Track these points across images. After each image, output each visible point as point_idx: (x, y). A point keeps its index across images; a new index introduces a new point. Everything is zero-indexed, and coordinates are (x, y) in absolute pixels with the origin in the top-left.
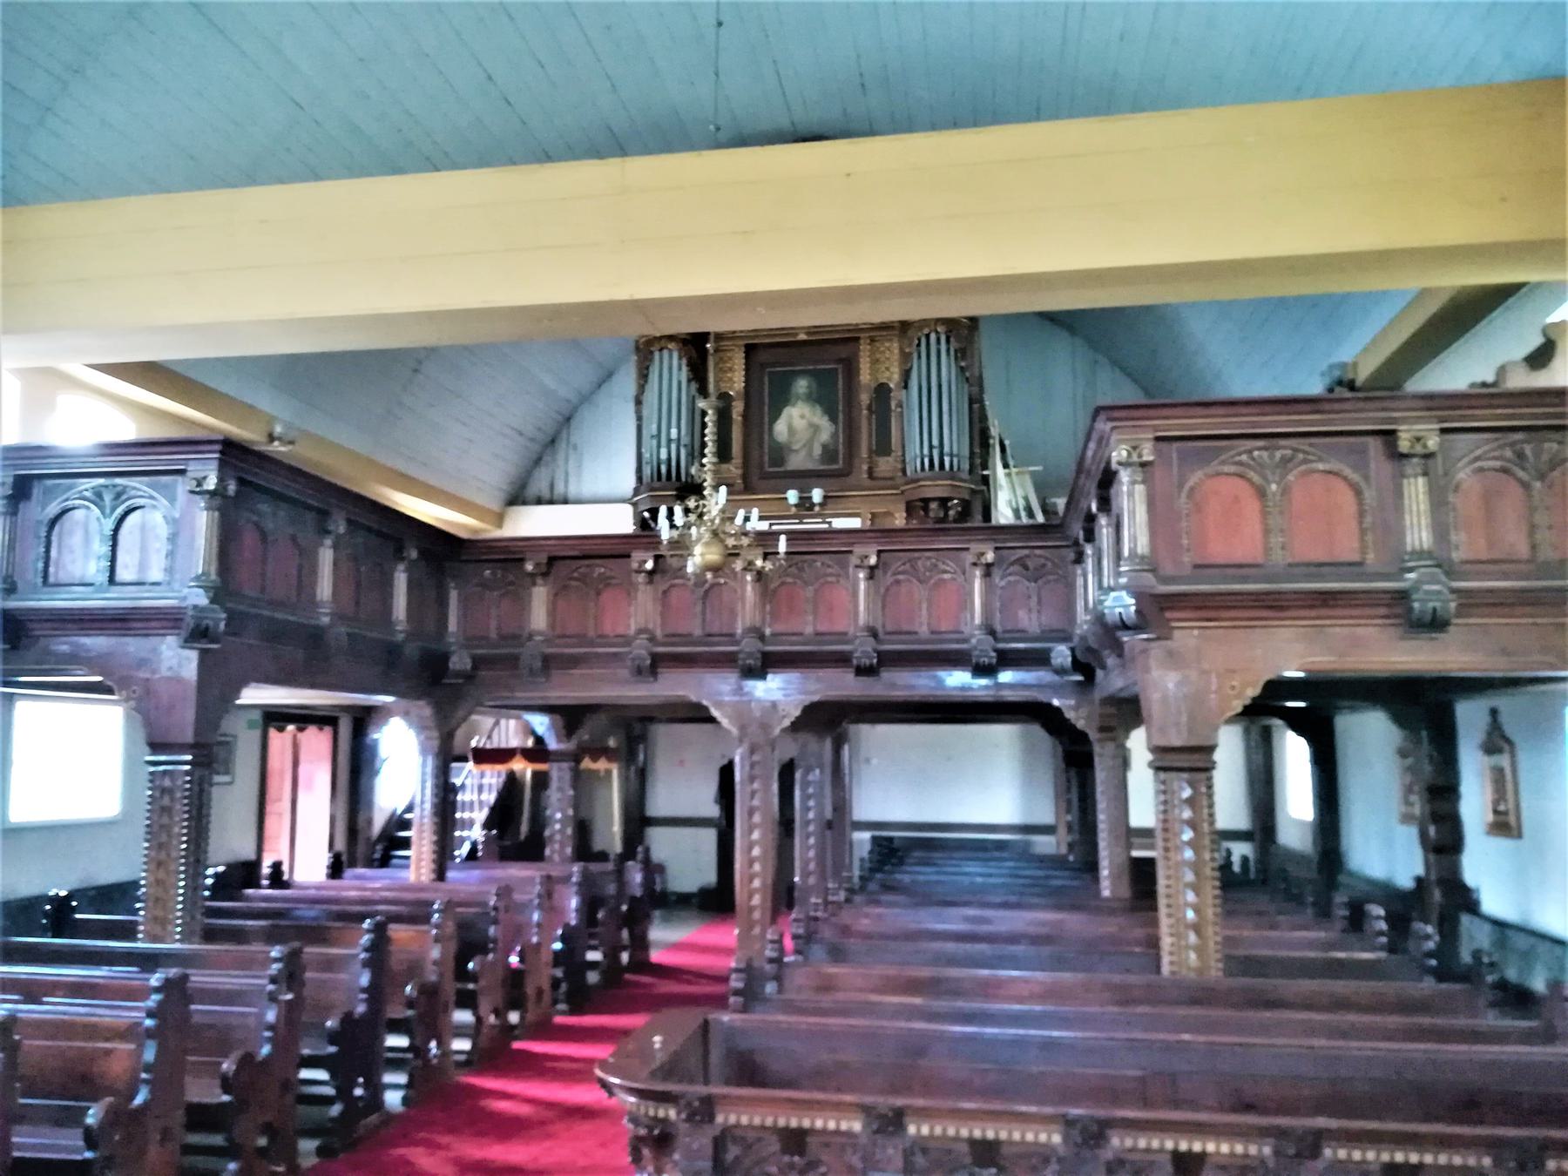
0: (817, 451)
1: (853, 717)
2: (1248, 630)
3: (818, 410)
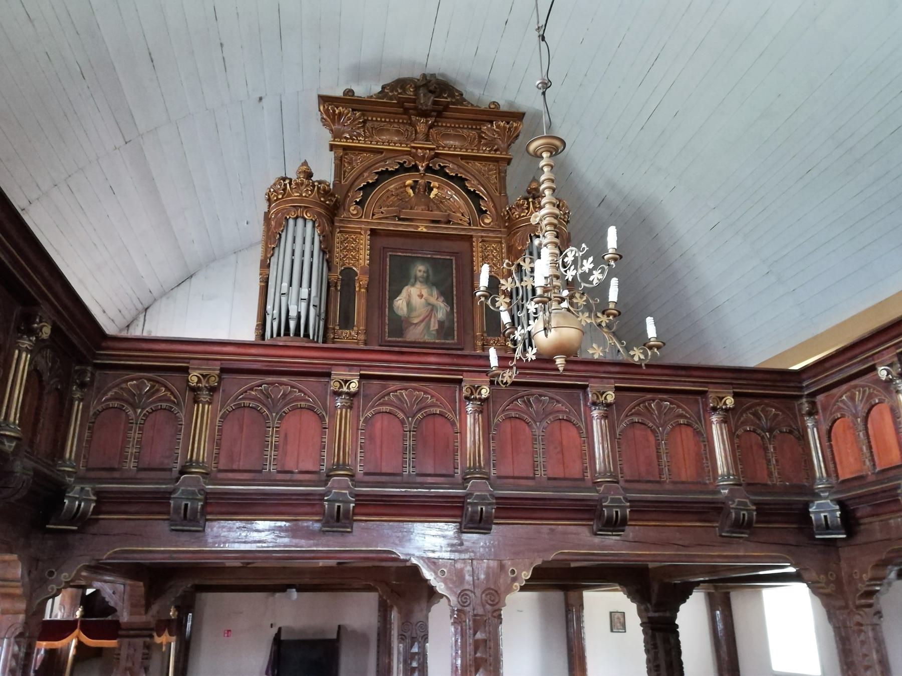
0: (434, 326)
2: (663, 527)
3: (435, 292)
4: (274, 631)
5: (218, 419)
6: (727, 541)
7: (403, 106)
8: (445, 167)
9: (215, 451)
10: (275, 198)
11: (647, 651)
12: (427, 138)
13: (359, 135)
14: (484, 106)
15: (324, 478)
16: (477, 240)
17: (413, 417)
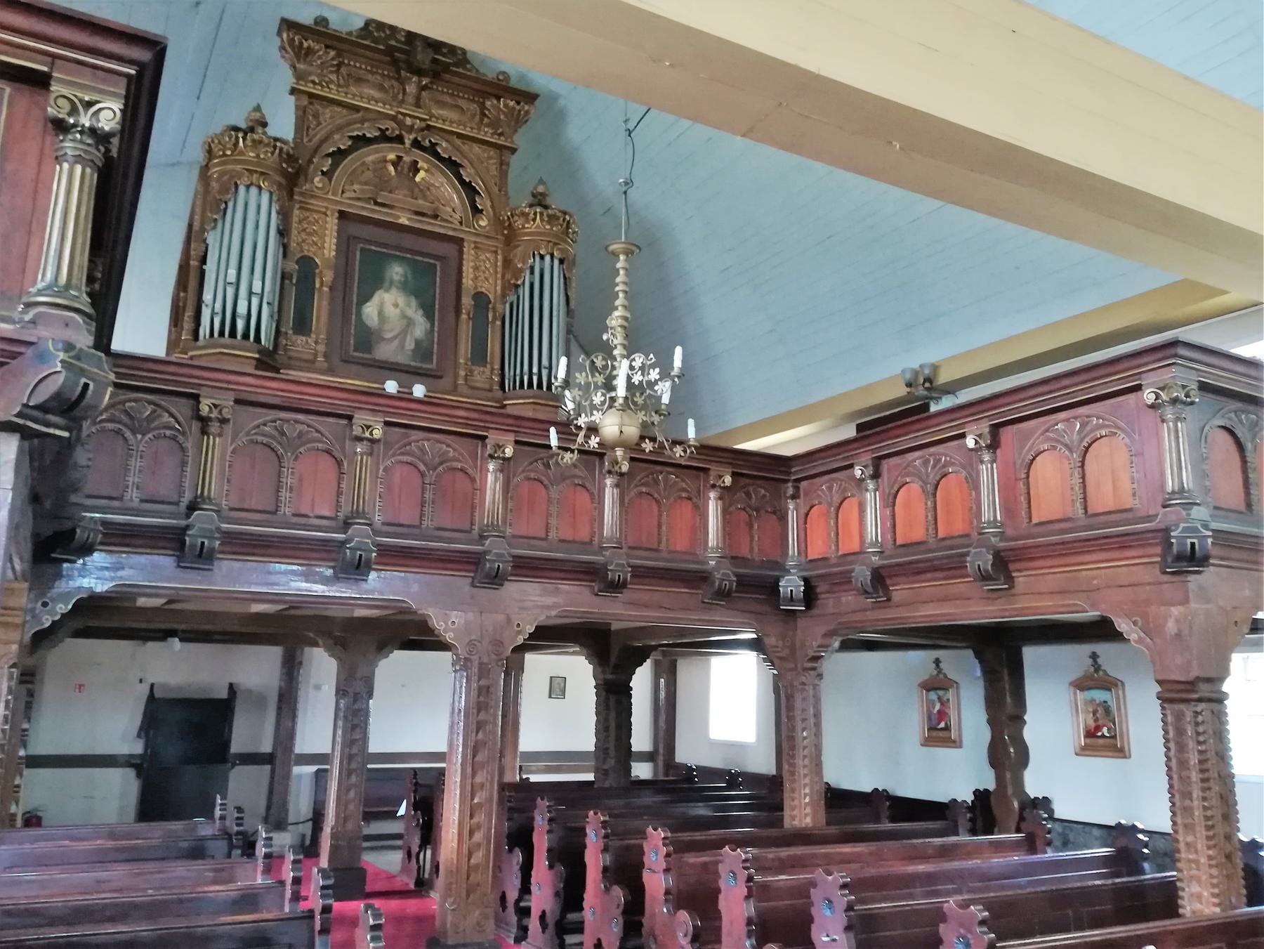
0: (410, 345)
3: (414, 303)
4: (144, 690)
5: (229, 453)
6: (707, 606)
7: (392, 56)
8: (437, 144)
9: (226, 488)
11: (597, 714)
12: (418, 104)
13: (332, 81)
14: (491, 76)
15: (341, 524)
17: (435, 469)
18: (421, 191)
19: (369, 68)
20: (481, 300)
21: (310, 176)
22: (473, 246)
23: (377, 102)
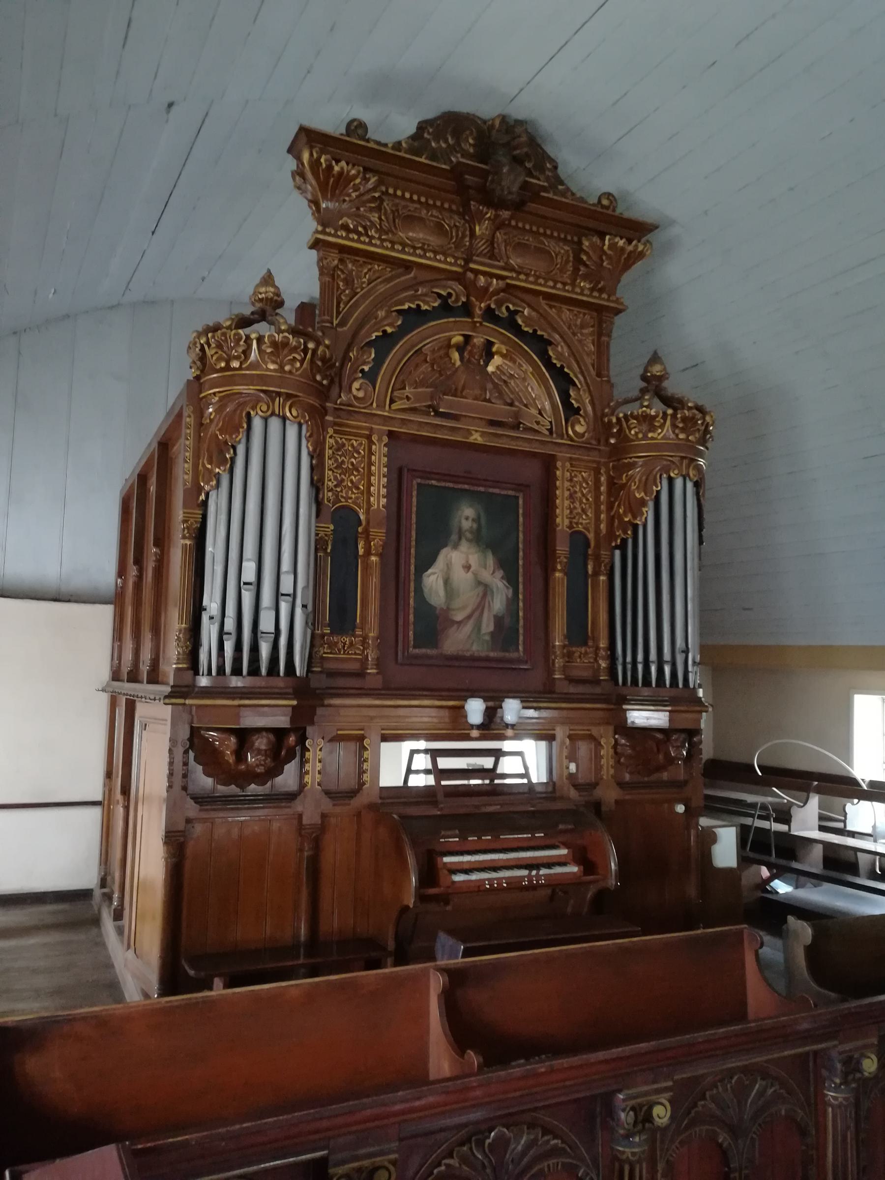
0: (488, 626)
1: (169, 860)
3: (490, 560)
8: (516, 312)
10: (223, 364)
16: (563, 466)
18: (496, 386)
19: (541, 230)
20: (578, 540)
21: (345, 383)
22: (568, 464)
23: (436, 253)
